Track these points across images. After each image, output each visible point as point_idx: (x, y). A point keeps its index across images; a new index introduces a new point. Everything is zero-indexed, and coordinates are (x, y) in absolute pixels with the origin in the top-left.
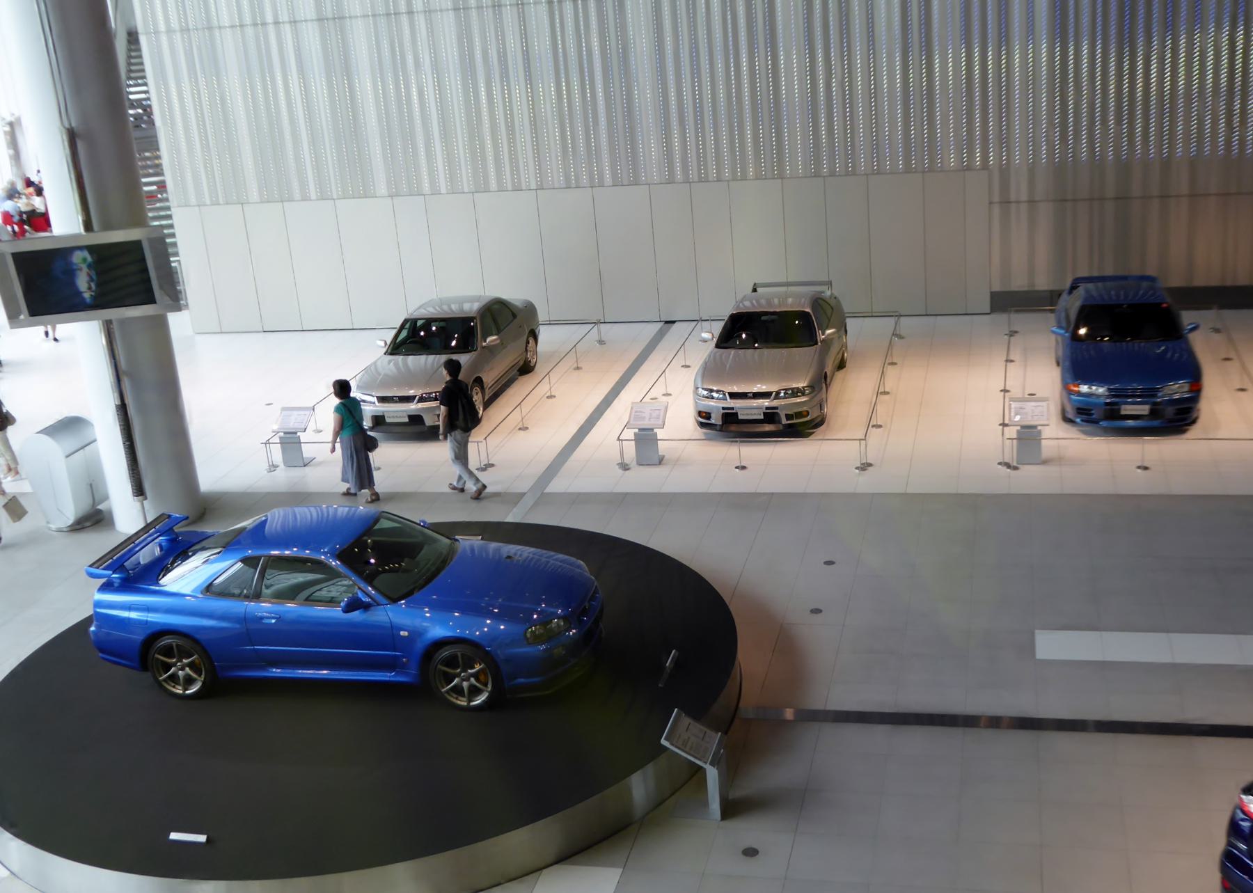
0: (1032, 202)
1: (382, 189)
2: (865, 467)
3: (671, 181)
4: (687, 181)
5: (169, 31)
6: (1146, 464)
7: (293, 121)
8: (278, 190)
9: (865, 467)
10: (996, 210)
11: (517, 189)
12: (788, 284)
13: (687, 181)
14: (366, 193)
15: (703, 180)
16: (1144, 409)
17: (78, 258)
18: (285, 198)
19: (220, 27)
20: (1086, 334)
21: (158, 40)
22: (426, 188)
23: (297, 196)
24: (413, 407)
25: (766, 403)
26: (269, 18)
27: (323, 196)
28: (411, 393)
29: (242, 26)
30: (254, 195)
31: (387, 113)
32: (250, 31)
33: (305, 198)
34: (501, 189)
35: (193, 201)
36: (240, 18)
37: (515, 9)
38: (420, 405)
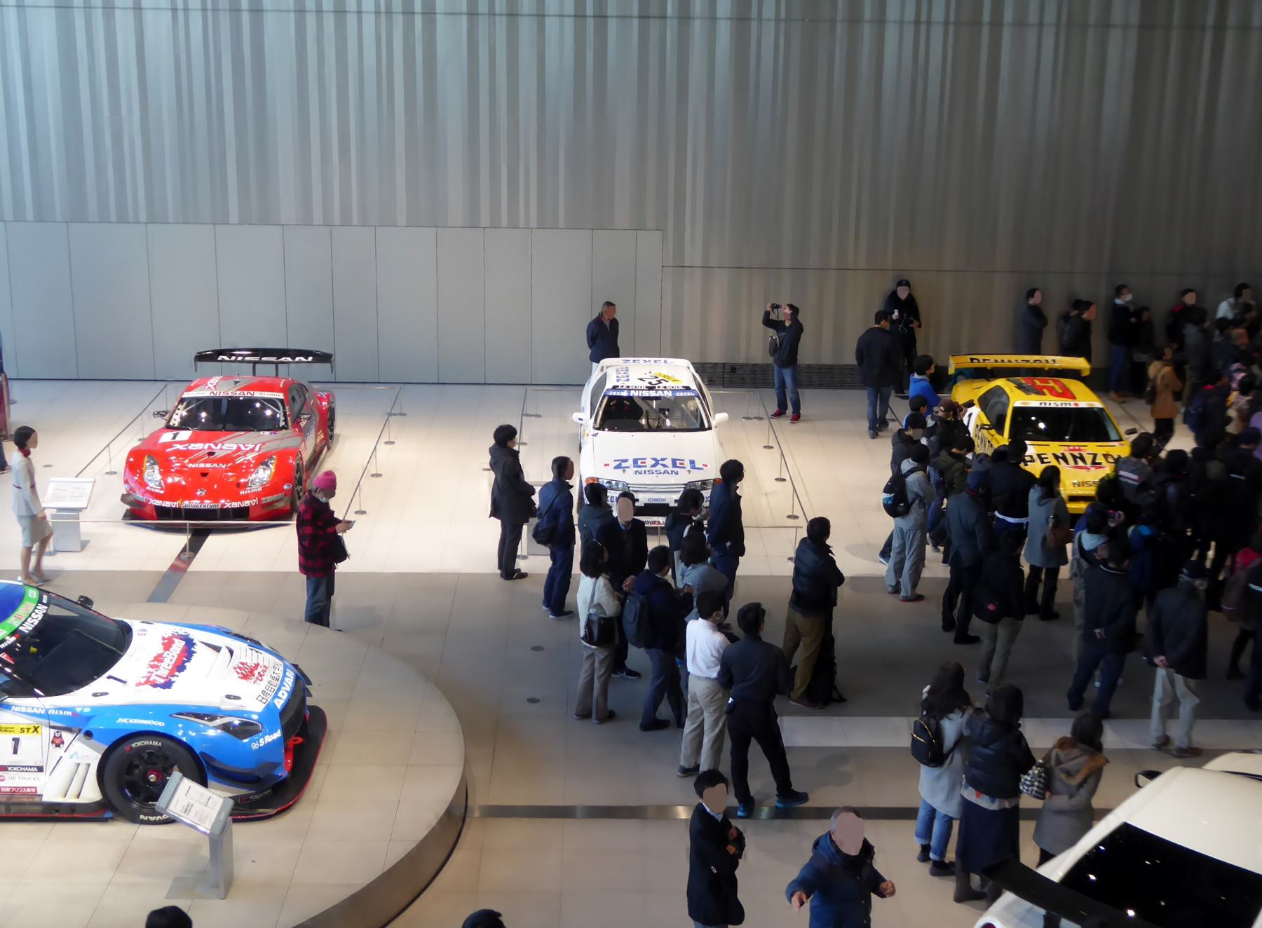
3: (307, 222)
4: (328, 223)
13: (328, 223)
15: (346, 222)
17: (1023, 520)
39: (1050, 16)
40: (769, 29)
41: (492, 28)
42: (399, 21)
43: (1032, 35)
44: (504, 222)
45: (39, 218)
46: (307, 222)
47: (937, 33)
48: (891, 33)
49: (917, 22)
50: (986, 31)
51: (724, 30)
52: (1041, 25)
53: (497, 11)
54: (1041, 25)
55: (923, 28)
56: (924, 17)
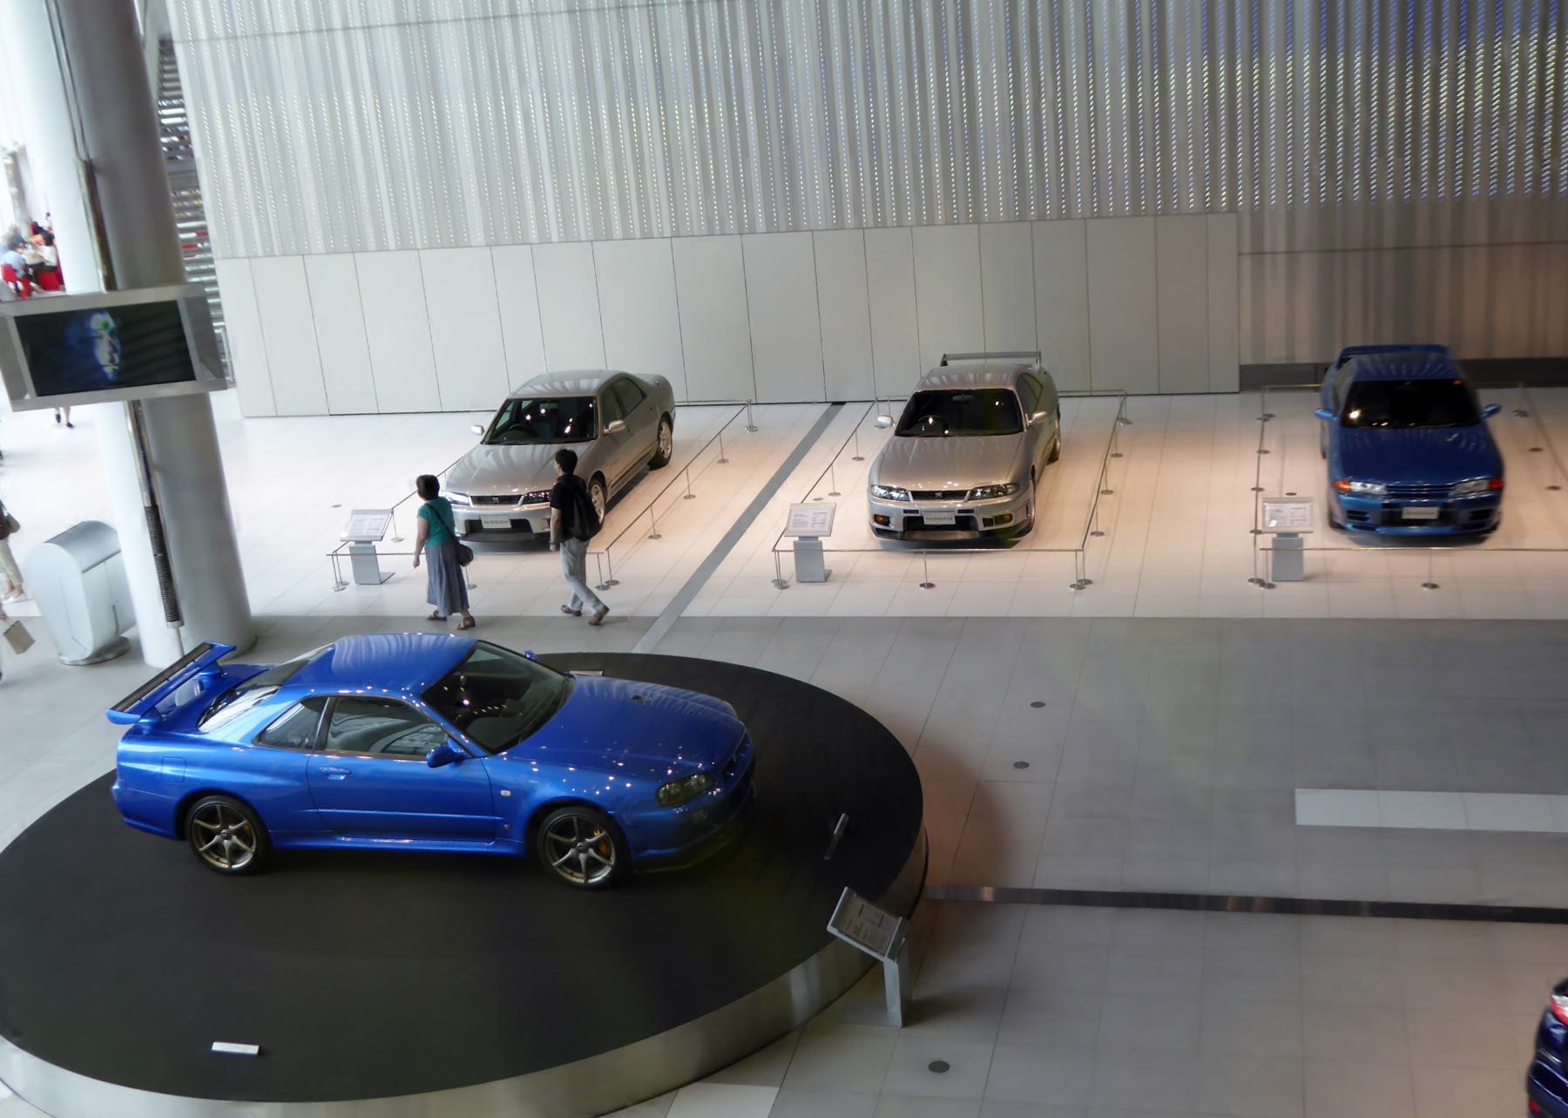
0: (1291, 253)
1: (478, 237)
2: (1082, 584)
3: (839, 226)
4: (860, 226)
5: (212, 39)
6: (1434, 581)
7: (366, 151)
8: (348, 238)
9: (1082, 584)
10: (1247, 263)
11: (647, 236)
12: (986, 356)
13: (860, 226)
14: (458, 242)
15: (880, 225)
16: (1432, 513)
18: (357, 248)
19: (275, 34)
20: (1359, 419)
21: (197, 50)
22: (533, 235)
23: (372, 245)
24: (517, 509)
25: (959, 504)
26: (337, 23)
27: (404, 246)
28: (515, 491)
29: (302, 32)
30: (318, 244)
31: (484, 142)
32: (312, 39)
33: (382, 248)
34: (627, 237)
35: (242, 251)
36: (301, 22)
37: (644, 11)
38: (526, 507)
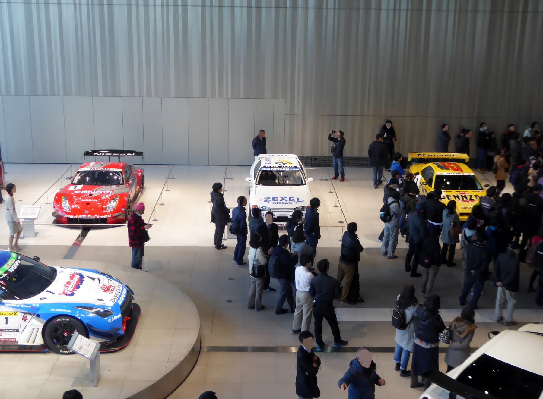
3: (132, 95)
4: (141, 96)
13: (141, 96)
15: (149, 96)
39: (452, 7)
40: (331, 13)
41: (212, 12)
42: (171, 9)
43: (444, 15)
44: (217, 96)
45: (17, 94)
46: (132, 95)
47: (403, 14)
48: (383, 14)
49: (395, 10)
50: (424, 13)
51: (312, 13)
52: (448, 11)
53: (214, 5)
54: (448, 11)
55: (397, 12)
56: (397, 7)
